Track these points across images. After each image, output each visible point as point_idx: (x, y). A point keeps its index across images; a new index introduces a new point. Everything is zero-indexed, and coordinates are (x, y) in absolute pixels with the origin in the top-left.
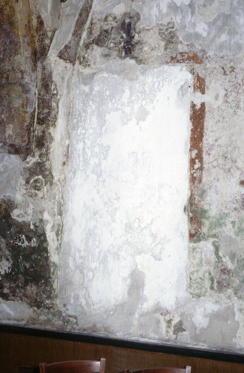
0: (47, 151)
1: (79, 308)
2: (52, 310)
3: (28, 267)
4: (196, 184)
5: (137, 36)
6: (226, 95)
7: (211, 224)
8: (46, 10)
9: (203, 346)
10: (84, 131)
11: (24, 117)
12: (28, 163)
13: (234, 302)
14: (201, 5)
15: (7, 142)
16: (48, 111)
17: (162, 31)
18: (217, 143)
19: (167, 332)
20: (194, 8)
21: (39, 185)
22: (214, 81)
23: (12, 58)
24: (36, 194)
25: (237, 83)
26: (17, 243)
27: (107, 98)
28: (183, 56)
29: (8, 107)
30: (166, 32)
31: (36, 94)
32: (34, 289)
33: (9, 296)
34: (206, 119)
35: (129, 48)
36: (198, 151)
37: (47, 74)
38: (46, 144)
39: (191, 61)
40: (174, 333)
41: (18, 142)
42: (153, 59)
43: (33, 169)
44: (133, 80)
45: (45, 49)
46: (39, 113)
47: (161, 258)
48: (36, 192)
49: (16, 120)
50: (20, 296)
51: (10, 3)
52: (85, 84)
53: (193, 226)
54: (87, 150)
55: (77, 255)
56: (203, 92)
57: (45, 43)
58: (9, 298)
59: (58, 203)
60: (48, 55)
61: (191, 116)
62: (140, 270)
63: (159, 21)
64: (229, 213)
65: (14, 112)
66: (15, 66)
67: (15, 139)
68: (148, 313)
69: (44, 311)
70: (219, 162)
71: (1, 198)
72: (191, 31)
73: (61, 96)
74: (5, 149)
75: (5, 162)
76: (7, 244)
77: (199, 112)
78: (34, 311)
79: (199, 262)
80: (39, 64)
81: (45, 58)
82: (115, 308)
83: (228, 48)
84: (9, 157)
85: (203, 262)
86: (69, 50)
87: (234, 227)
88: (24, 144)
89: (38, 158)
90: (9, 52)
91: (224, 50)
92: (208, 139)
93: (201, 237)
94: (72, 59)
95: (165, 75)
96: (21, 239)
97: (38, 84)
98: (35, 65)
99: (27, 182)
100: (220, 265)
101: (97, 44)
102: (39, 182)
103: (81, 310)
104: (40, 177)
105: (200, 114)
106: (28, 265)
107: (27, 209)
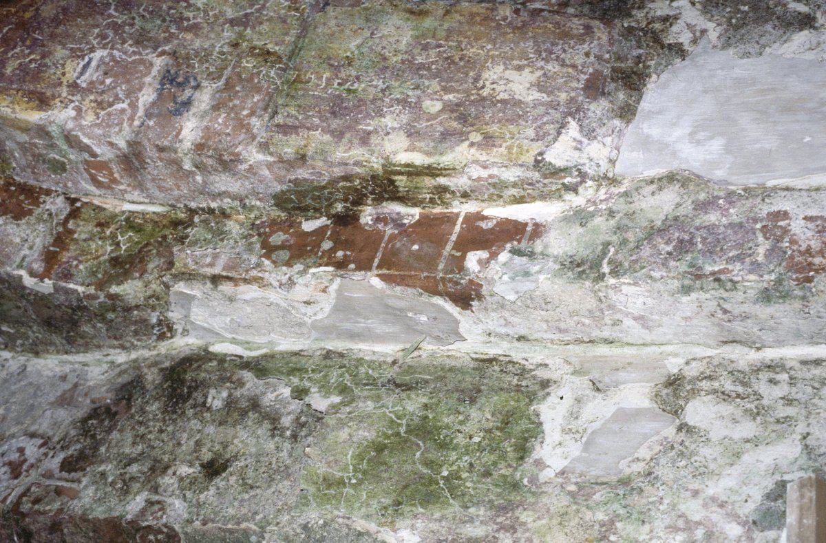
23: (191, 15)
65: (433, 53)
67: (563, 65)
90: (159, 22)
92: (631, 342)
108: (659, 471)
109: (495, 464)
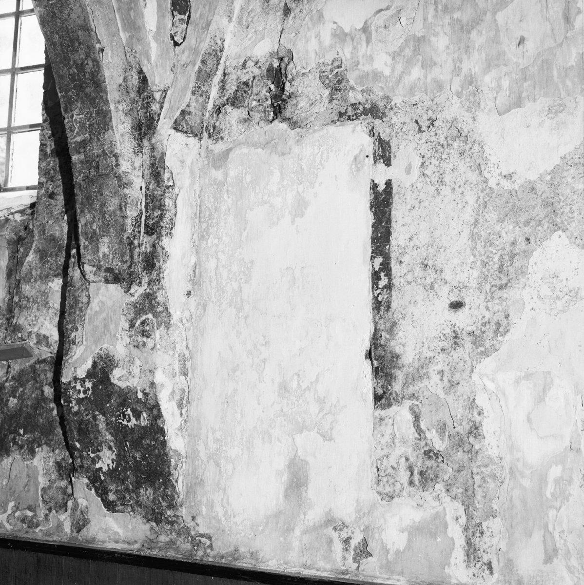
0: (158, 275)
1: (213, 522)
2: (176, 525)
3: (139, 458)
4: (381, 313)
5: (287, 85)
6: (423, 164)
7: (407, 375)
8: (148, 60)
9: (398, 580)
10: (216, 241)
11: (123, 225)
12: (132, 295)
13: (445, 505)
14: (380, 27)
15: (101, 266)
16: (160, 212)
17: (324, 74)
18: (412, 244)
19: (344, 558)
20: (370, 33)
21: (148, 328)
22: (403, 144)
24: (144, 342)
25: (439, 143)
26: (120, 421)
27: (248, 186)
28: (355, 109)
29: (101, 212)
30: (331, 74)
31: (143, 188)
32: (150, 494)
33: (116, 505)
34: (394, 206)
35: (279, 106)
36: (383, 258)
37: (158, 156)
38: (157, 265)
39: (367, 115)
40: (355, 560)
41: (117, 264)
42: (312, 119)
43: (140, 304)
44: (285, 154)
45: (153, 118)
46: (147, 218)
47: (333, 437)
48: (145, 339)
49: (112, 230)
50: (131, 505)
51: (92, 54)
52: (217, 168)
53: (379, 381)
54: (221, 269)
55: (211, 437)
56: (388, 164)
57: (152, 110)
58: (117, 509)
59: (179, 356)
60: (158, 128)
61: (371, 203)
62: (302, 458)
63: (320, 59)
64: (434, 357)
66: (106, 148)
67: (112, 259)
68: (315, 528)
69: (165, 527)
70: (416, 274)
71: (96, 352)
72: (367, 68)
73: (180, 188)
74: (99, 276)
75: (101, 297)
76: (107, 424)
77: (384, 196)
78: (152, 528)
79: (389, 441)
80: (146, 143)
81: (154, 133)
82: (265, 521)
83: (423, 90)
84: (106, 288)
85: (397, 441)
86: (187, 117)
87: (442, 380)
88: (125, 267)
89: (146, 286)
91: (416, 93)
93: (392, 400)
94: (196, 131)
95: (331, 141)
96: (125, 415)
97: (146, 173)
98: (139, 145)
99: (132, 326)
100: (423, 443)
101: (233, 104)
102: (148, 324)
103: (216, 525)
104: (150, 316)
105: (385, 198)
106: (138, 456)
107: (132, 367)
108: (50, 310)
109: (53, 270)
